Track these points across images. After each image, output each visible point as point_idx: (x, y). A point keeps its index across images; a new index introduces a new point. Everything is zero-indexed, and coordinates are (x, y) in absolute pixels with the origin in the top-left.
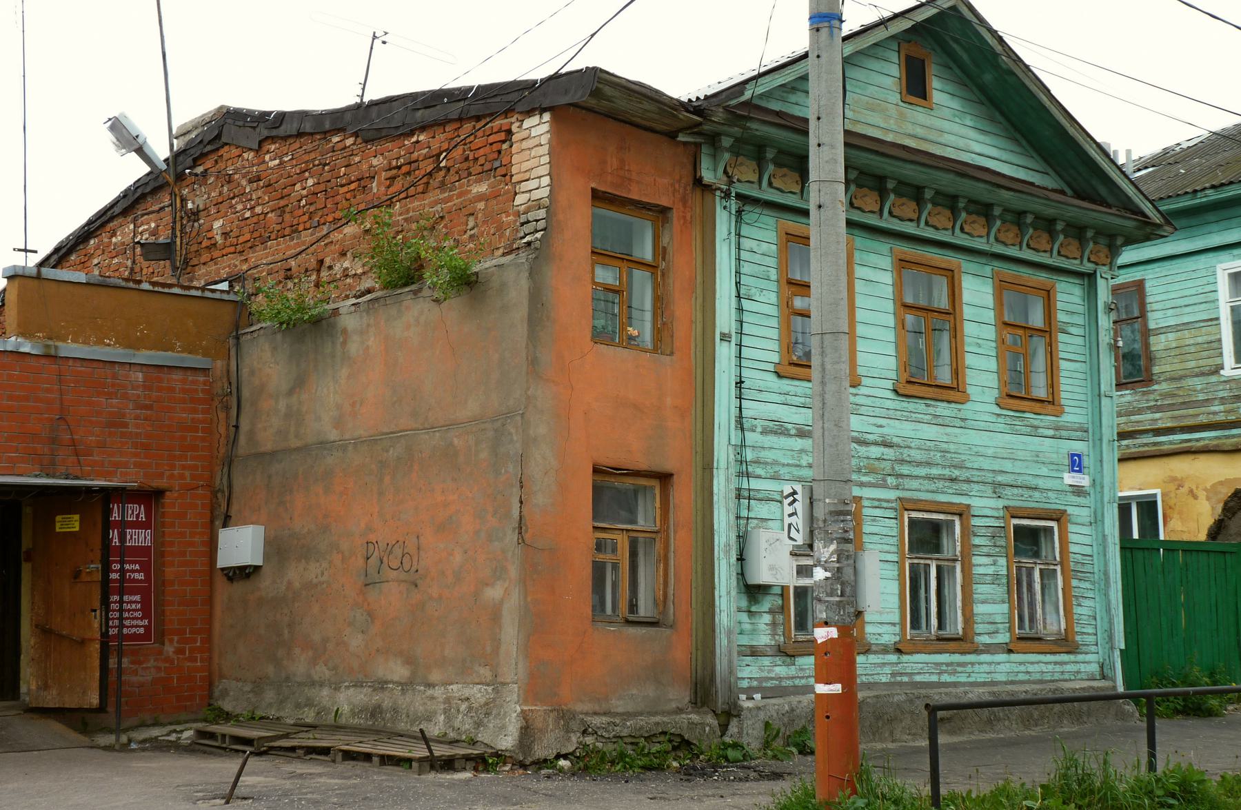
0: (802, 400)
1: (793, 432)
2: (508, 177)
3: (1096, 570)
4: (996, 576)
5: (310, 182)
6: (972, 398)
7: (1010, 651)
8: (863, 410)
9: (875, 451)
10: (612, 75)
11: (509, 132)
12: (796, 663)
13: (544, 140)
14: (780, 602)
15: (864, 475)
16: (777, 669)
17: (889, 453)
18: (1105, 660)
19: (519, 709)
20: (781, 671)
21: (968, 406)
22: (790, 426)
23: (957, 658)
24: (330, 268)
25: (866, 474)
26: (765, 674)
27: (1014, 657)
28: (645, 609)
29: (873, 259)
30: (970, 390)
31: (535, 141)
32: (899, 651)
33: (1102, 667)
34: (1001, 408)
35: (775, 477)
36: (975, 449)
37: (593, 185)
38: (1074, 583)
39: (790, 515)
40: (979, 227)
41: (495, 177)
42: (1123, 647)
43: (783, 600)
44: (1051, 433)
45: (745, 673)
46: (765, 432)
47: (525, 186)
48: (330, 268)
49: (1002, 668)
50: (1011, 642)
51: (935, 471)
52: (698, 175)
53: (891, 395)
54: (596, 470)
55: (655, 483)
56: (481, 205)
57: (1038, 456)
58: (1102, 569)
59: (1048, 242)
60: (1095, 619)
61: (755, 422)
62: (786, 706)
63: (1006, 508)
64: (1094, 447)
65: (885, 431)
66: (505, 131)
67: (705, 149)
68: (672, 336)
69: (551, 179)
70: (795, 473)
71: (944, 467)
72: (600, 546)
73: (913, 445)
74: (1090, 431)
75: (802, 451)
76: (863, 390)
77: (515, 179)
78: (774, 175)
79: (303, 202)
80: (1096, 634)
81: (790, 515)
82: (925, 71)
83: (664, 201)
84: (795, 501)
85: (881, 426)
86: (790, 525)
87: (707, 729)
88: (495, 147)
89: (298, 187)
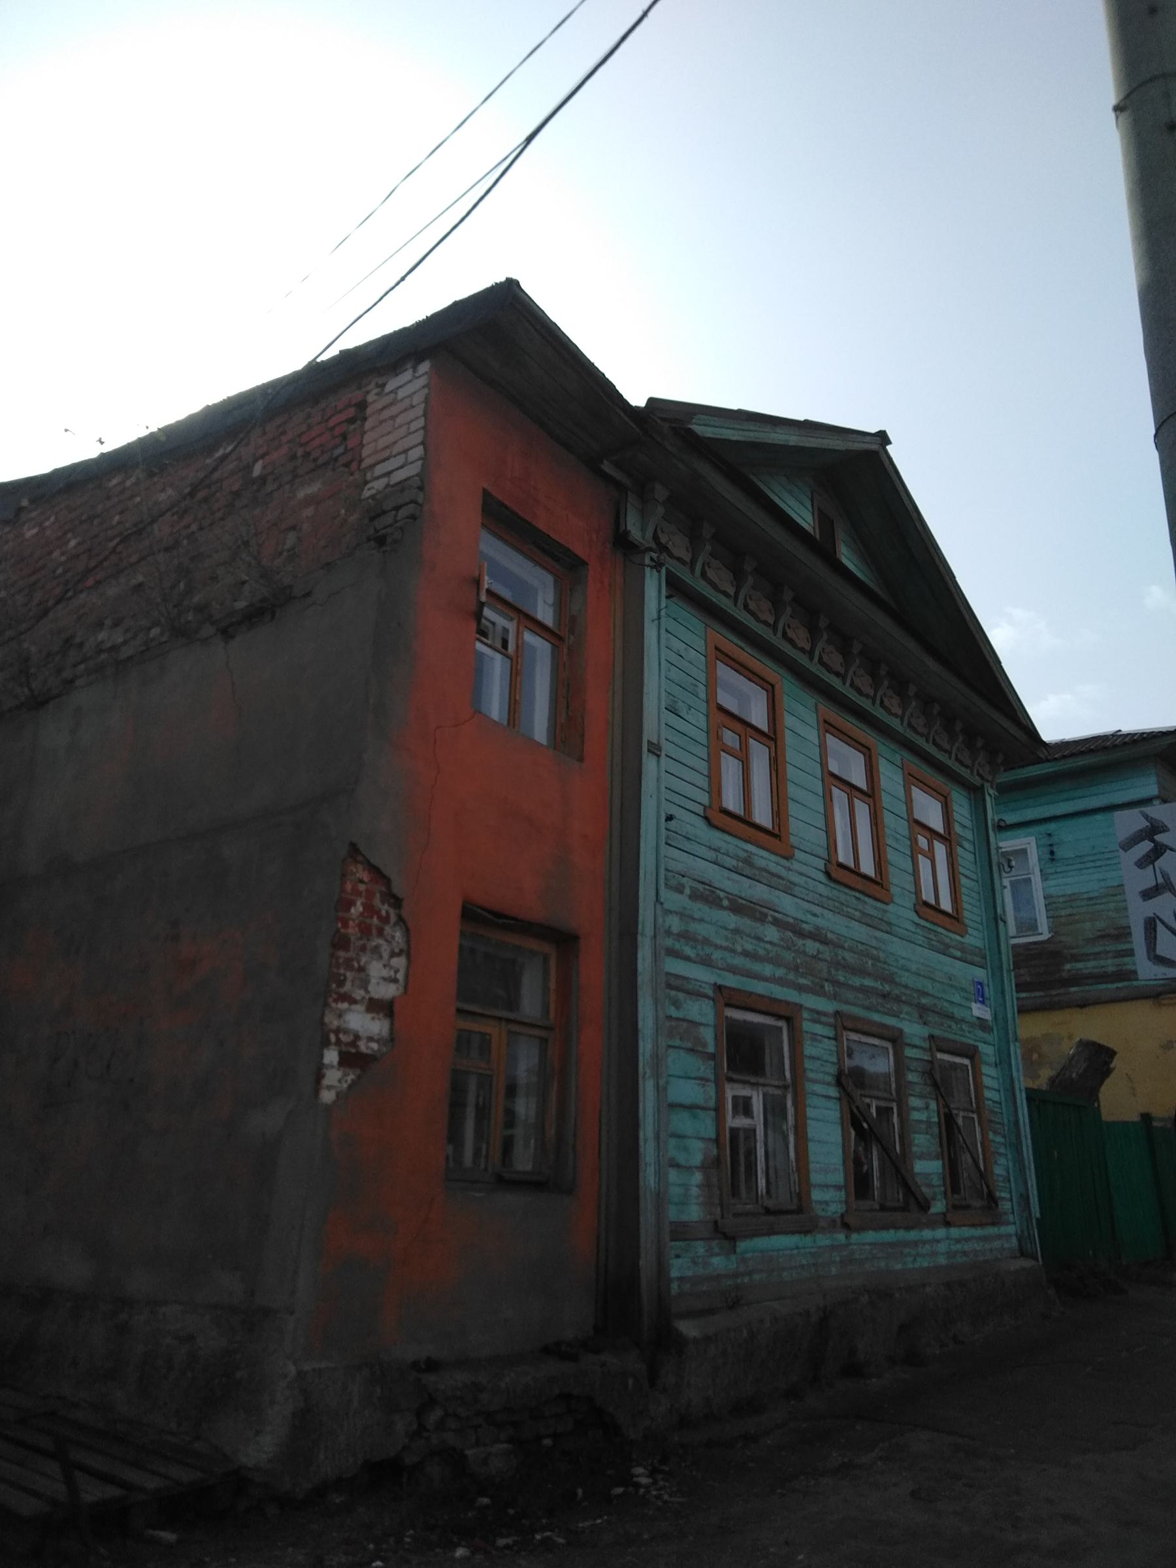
0: (734, 862)
1: (726, 903)
2: (354, 465)
3: (1006, 1121)
4: (928, 1123)
5: (73, 543)
6: (896, 900)
7: (948, 1224)
8: (797, 891)
9: (811, 946)
10: (533, 301)
11: (362, 405)
12: (738, 1250)
13: (418, 399)
14: (715, 1151)
15: (802, 977)
16: (716, 1260)
17: (827, 952)
18: (1022, 1231)
19: (292, 1369)
20: (719, 1263)
21: (891, 908)
22: (722, 894)
23: (902, 1235)
24: (81, 645)
25: (803, 975)
26: (700, 1271)
27: (955, 1232)
28: (524, 1161)
29: (800, 709)
30: (894, 890)
31: (407, 402)
32: (846, 1226)
33: (1019, 1241)
34: (920, 917)
35: (707, 962)
36: (902, 962)
37: (486, 486)
38: (991, 1136)
39: (1148, 895)
40: (894, 704)
41: (333, 470)
42: (1038, 1215)
43: (718, 1147)
44: (958, 954)
45: (678, 1268)
46: (695, 896)
47: (380, 470)
48: (81, 645)
49: (942, 1248)
50: (948, 1210)
51: (868, 982)
52: (622, 528)
53: (822, 877)
54: (471, 914)
55: (547, 948)
56: (309, 512)
57: (951, 980)
58: (1012, 1119)
59: (949, 743)
60: (1009, 1181)
61: (684, 880)
62: (745, 1331)
63: (932, 1037)
64: (993, 974)
65: (820, 922)
66: (355, 405)
67: (632, 499)
68: (582, 736)
69: (425, 449)
70: (730, 961)
71: (876, 978)
72: (463, 1041)
73: (846, 945)
74: (988, 957)
75: (736, 931)
76: (796, 866)
77: (364, 465)
78: (708, 563)
79: (60, 571)
80: (1011, 1200)
81: (1148, 895)
82: (833, 529)
83: (579, 550)
84: (1159, 851)
85: (815, 915)
86: (1151, 925)
87: (630, 1382)
88: (337, 431)
89: (56, 554)
